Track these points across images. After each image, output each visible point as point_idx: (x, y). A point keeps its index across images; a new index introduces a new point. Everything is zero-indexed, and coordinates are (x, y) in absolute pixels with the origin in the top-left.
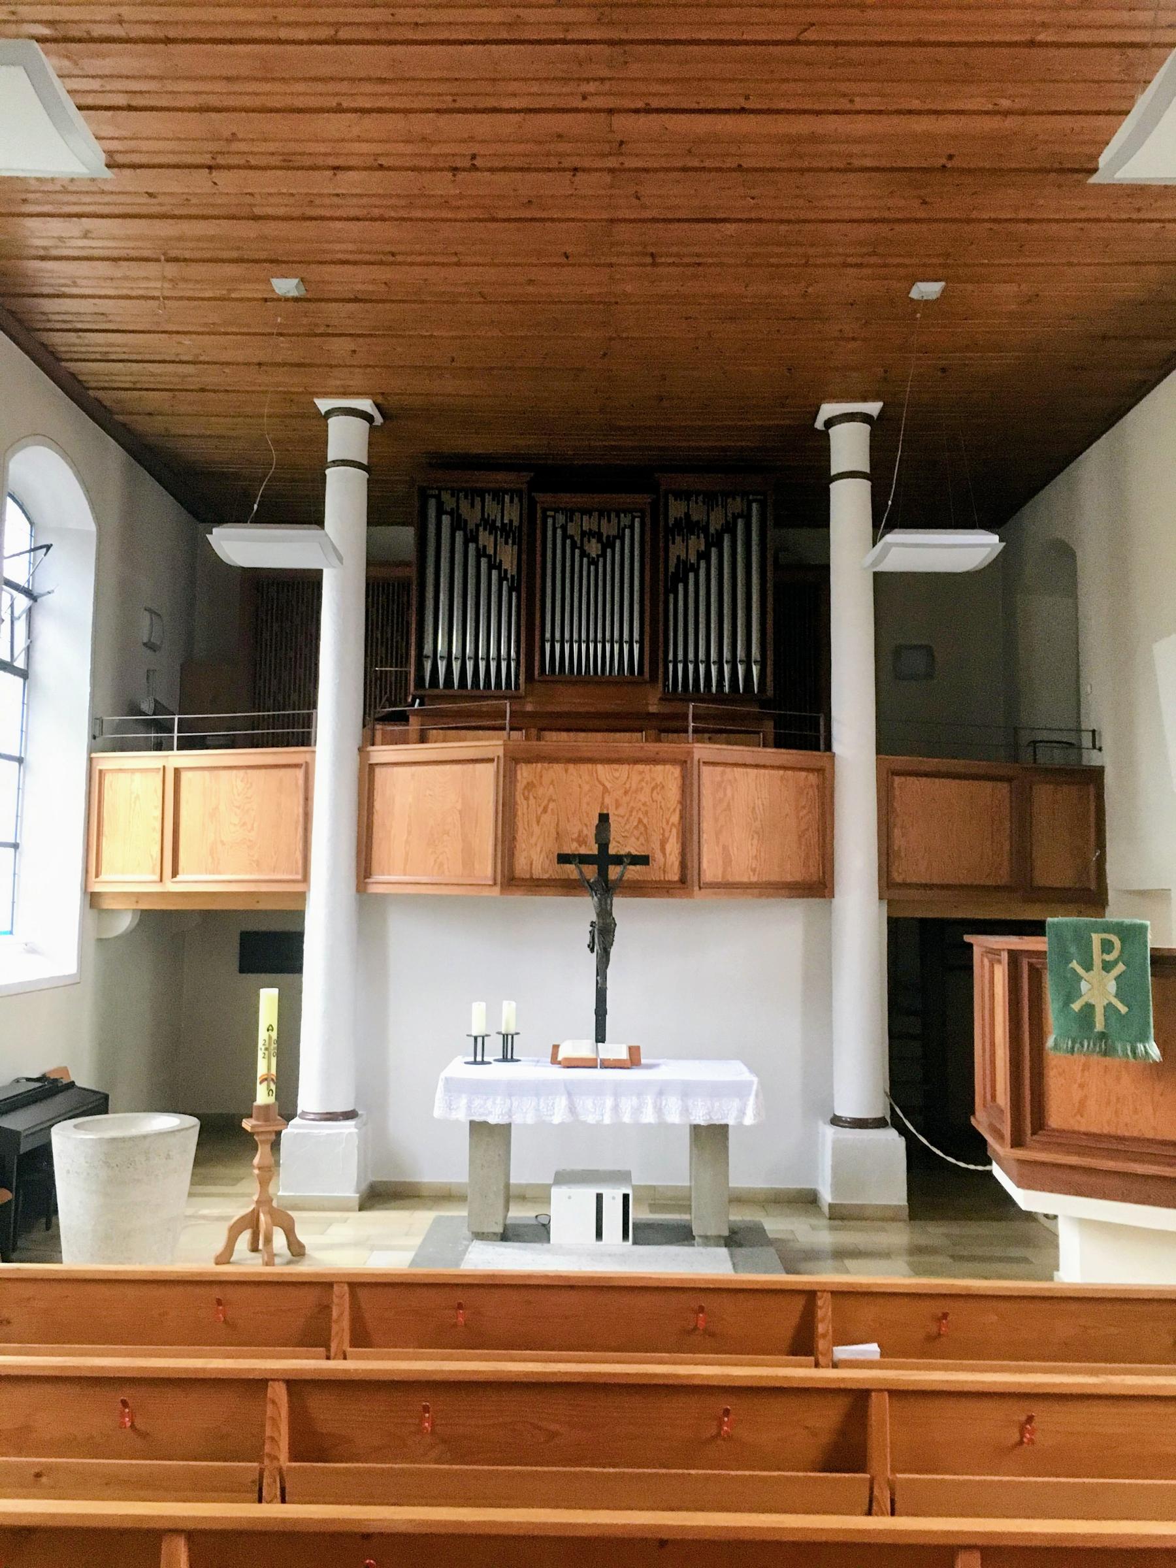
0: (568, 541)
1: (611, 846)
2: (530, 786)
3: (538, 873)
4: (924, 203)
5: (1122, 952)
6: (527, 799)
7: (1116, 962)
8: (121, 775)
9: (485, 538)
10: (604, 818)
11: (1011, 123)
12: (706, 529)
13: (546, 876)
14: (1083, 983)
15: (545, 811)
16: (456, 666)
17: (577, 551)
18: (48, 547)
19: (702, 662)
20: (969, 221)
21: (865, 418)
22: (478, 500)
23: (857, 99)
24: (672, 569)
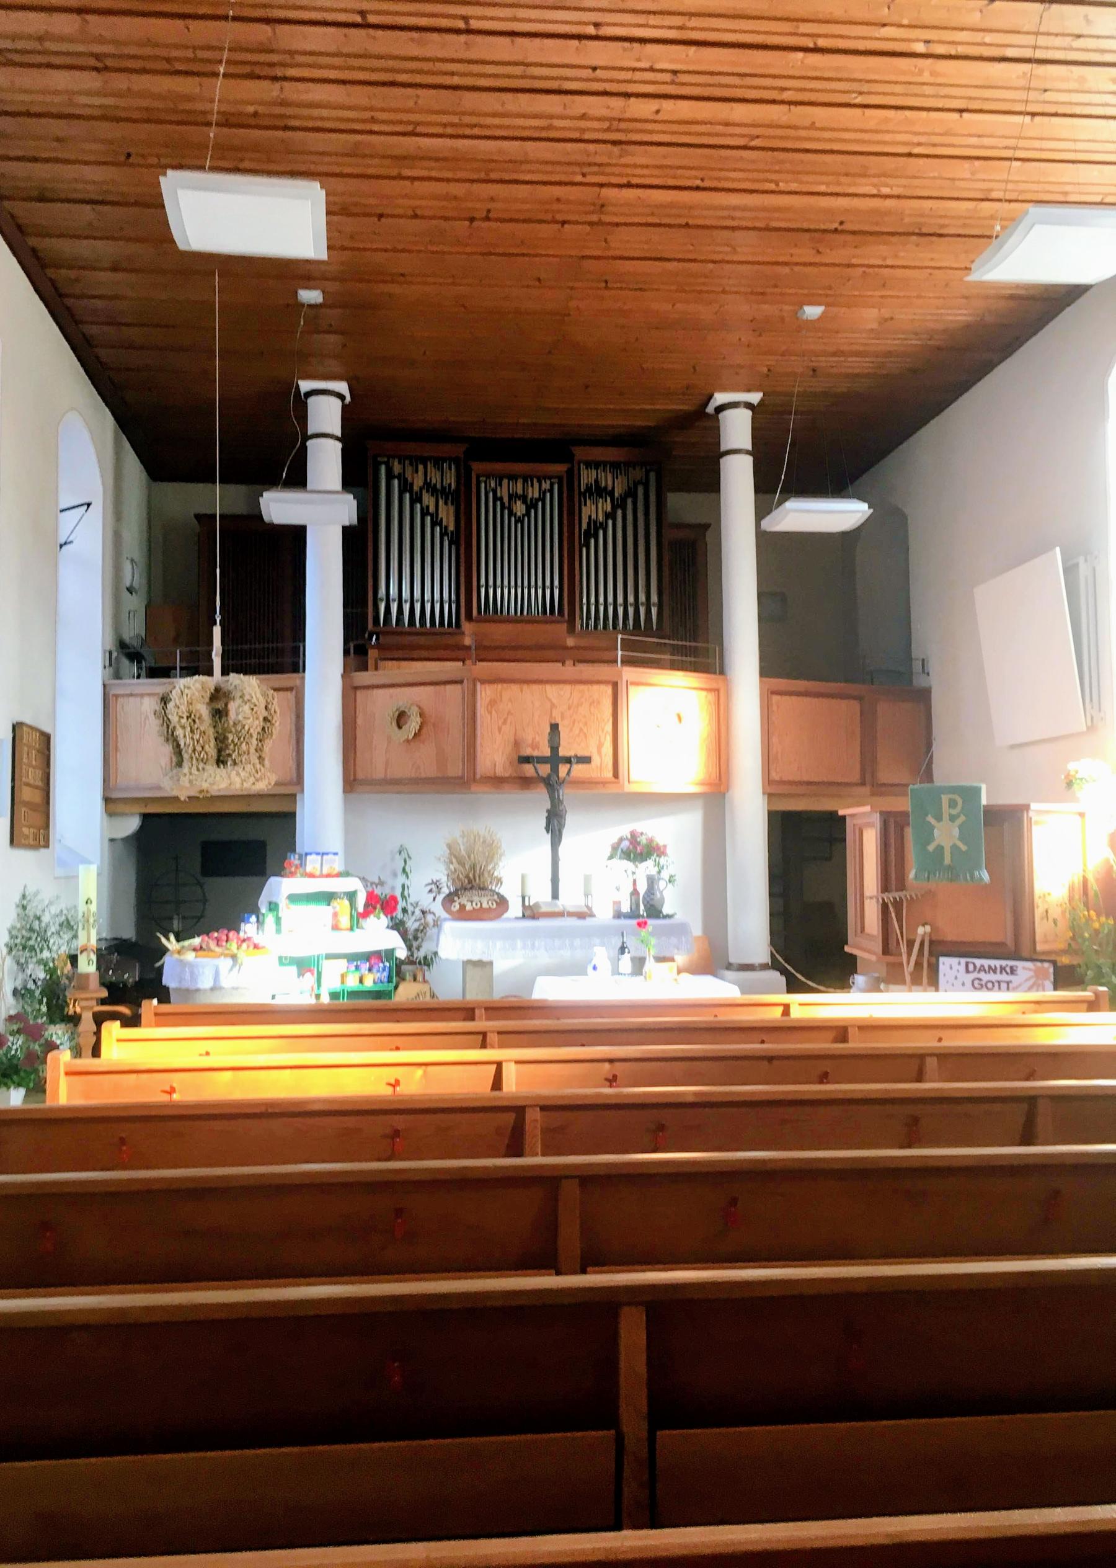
0: (498, 503)
1: (560, 749)
2: (492, 703)
3: (500, 771)
4: (818, 252)
5: (962, 808)
6: (490, 713)
7: (958, 816)
8: (131, 699)
9: (428, 500)
10: (554, 727)
11: (889, 203)
12: (611, 494)
13: (507, 775)
14: (935, 831)
15: (505, 722)
16: (394, 607)
17: (506, 512)
18: (89, 505)
19: (642, 604)
20: (849, 266)
21: (749, 405)
22: (421, 467)
23: (781, 184)
24: (584, 526)
